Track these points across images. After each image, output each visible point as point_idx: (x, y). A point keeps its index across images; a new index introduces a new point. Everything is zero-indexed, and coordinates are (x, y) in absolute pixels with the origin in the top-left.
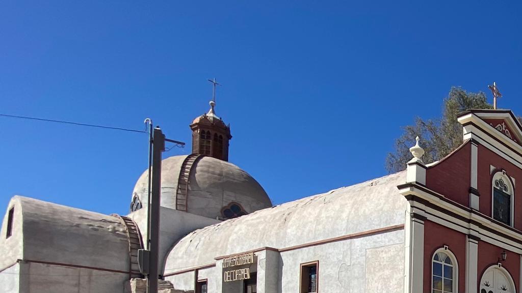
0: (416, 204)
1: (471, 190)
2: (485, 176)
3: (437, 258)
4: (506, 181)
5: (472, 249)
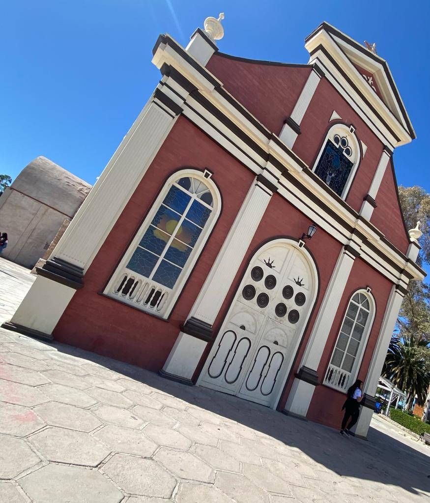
1: (367, 198)
4: (352, 143)
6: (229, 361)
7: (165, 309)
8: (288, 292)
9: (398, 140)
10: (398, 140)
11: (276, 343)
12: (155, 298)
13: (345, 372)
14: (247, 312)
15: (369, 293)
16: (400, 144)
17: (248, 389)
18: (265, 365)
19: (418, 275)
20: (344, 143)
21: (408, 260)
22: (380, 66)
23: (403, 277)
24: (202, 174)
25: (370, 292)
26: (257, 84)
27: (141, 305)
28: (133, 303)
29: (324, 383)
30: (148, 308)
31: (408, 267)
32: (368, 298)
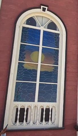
12: (46, 115)
30: (44, 125)
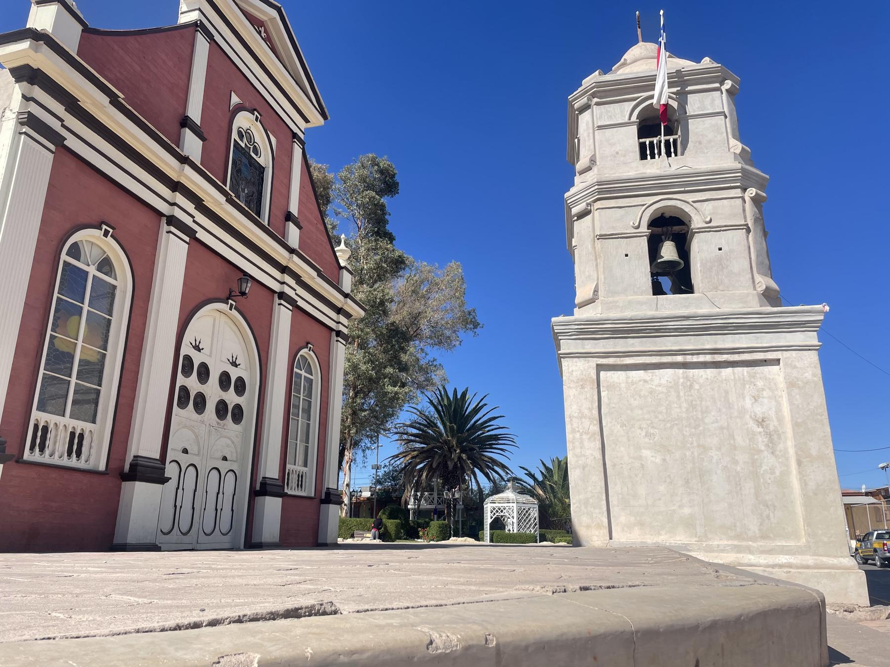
0: (38, 93)
2: (220, 113)
3: (75, 251)
5: (173, 254)
6: (219, 508)
7: (96, 457)
8: (225, 380)
9: (307, 121)
10: (307, 121)
11: (225, 459)
12: (76, 443)
13: (80, 425)
14: (185, 427)
15: (311, 353)
16: (309, 125)
17: (223, 534)
18: (178, 489)
19: (357, 312)
20: (250, 139)
21: (184, 160)
22: (274, 13)
23: (342, 319)
24: (98, 233)
25: (236, 309)
26: (138, 69)
27: (65, 462)
28: (56, 460)
29: (27, 455)
30: (73, 462)
31: (349, 306)
32: (309, 360)
